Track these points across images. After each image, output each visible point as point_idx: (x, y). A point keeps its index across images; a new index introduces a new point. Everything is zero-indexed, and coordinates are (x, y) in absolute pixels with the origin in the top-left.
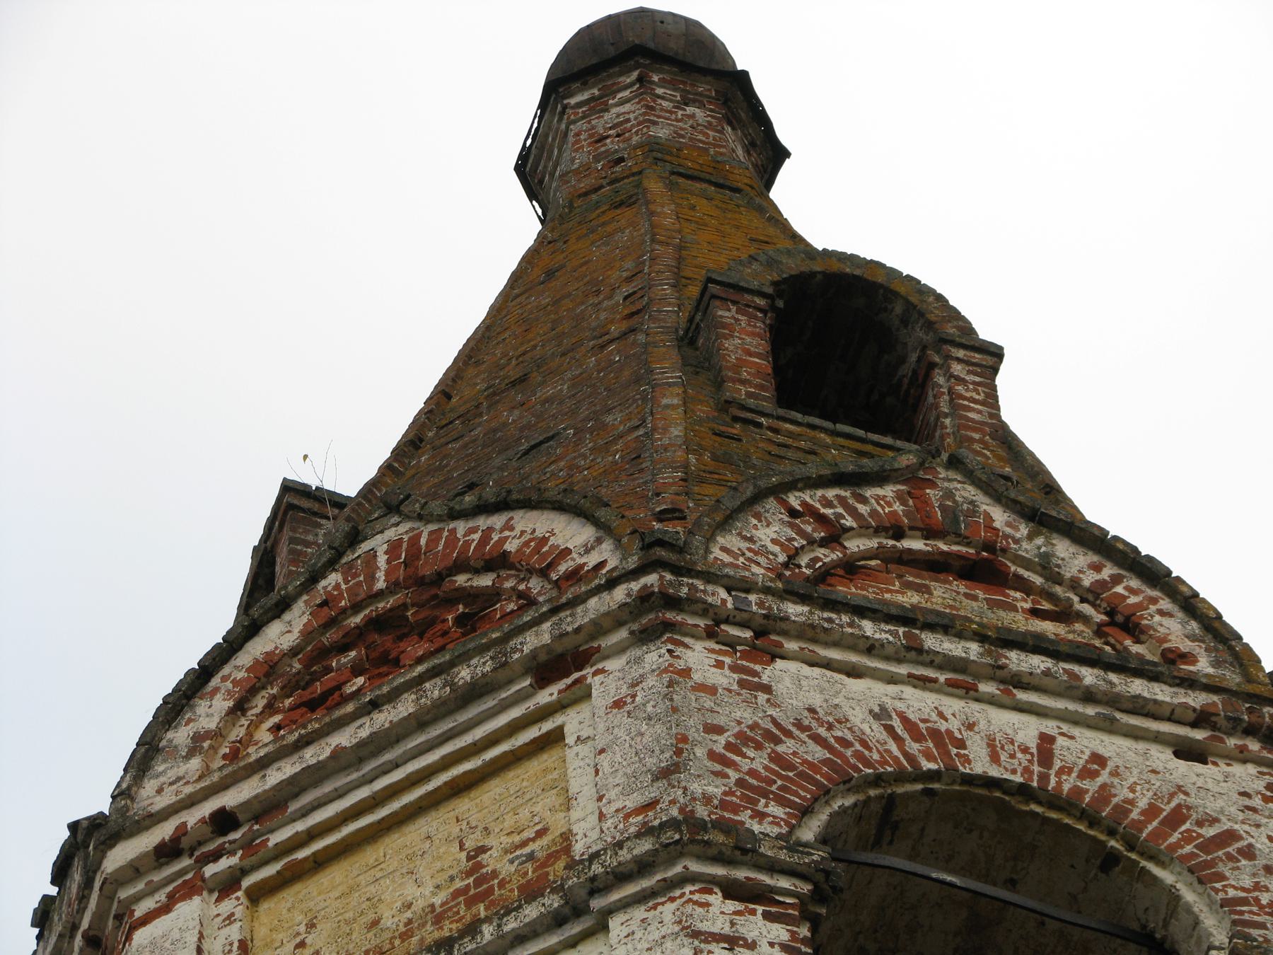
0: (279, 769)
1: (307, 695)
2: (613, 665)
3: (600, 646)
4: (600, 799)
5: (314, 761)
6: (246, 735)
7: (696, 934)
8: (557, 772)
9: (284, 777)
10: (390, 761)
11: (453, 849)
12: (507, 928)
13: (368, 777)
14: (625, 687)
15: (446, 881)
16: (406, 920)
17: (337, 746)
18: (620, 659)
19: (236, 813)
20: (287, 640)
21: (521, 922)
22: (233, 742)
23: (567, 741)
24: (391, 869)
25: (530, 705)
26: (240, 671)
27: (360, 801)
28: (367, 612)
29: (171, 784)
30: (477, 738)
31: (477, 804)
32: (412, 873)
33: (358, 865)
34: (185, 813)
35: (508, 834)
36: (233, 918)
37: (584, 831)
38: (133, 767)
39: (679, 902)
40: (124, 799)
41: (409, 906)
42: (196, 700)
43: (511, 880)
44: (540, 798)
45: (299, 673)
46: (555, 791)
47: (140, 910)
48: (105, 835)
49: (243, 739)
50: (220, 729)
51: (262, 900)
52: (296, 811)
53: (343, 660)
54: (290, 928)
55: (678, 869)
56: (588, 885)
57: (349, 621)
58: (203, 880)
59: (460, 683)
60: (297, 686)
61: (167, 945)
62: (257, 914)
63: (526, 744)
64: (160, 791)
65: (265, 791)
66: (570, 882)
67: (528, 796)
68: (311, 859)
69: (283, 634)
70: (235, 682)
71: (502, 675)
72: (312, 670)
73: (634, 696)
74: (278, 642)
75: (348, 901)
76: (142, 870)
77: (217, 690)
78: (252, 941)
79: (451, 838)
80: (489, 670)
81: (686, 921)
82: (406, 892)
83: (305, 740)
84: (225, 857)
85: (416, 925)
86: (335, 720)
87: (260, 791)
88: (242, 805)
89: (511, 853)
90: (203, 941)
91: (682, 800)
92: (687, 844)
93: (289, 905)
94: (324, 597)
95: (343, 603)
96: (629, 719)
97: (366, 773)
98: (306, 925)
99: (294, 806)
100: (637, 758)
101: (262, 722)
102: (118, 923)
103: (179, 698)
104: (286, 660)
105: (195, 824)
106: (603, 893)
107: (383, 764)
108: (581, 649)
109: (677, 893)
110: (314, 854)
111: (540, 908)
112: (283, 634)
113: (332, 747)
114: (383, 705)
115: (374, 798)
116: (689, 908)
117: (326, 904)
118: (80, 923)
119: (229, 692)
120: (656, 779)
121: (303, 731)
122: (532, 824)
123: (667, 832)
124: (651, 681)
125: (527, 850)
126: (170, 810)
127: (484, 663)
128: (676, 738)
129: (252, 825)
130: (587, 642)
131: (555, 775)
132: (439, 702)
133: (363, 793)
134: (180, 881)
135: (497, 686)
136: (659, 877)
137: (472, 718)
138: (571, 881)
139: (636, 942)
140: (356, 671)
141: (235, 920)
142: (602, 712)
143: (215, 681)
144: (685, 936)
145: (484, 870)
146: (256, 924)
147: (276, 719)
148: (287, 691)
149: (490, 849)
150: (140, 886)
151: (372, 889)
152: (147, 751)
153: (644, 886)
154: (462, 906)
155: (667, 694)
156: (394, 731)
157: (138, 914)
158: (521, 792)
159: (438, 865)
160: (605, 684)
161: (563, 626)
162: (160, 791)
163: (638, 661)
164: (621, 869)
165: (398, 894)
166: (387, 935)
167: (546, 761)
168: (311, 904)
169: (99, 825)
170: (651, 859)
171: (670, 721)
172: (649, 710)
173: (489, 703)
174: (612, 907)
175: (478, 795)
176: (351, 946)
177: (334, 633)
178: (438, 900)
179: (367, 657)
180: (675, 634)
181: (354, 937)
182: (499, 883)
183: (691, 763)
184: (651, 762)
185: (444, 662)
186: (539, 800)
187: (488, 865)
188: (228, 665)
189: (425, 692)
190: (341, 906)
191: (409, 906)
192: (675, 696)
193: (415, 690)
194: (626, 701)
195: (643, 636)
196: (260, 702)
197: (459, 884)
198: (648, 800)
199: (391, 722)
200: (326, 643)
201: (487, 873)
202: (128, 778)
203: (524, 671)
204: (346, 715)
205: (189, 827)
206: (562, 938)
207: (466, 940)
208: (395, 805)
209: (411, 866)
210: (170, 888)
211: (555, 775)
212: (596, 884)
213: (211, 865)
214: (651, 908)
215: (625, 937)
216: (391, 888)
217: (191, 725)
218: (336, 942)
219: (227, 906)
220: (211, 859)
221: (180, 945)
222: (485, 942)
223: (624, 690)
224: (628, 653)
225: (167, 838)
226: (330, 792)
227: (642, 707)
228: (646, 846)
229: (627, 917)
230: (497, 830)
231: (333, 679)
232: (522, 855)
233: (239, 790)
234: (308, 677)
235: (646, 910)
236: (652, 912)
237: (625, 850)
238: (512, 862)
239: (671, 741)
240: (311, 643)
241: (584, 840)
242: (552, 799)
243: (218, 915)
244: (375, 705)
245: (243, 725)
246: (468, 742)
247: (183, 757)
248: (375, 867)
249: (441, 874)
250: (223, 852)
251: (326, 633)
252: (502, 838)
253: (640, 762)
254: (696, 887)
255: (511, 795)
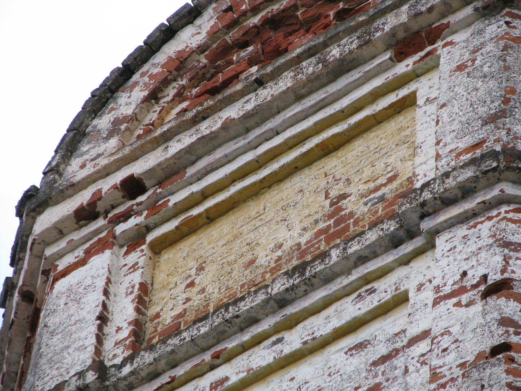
0: (179, 141)
1: (210, 85)
2: (459, 37)
3: (449, 22)
4: (438, 143)
5: (208, 132)
6: (158, 119)
7: (507, 245)
8: (410, 129)
9: (183, 147)
10: (272, 130)
11: (319, 198)
12: (350, 251)
13: (253, 144)
14: (467, 54)
15: (311, 224)
16: (276, 258)
17: (227, 118)
18: (466, 32)
19: (142, 179)
20: (197, 39)
21: (363, 244)
22: (147, 125)
23: (418, 103)
24: (269, 219)
25: (390, 75)
26: (156, 67)
27: (246, 164)
28: (263, 13)
29: (92, 160)
30: (344, 106)
31: (342, 162)
32: (285, 220)
33: (242, 218)
34: (100, 182)
35: (365, 183)
36: (136, 267)
37: (424, 172)
38: (62, 149)
39: (495, 219)
40: (53, 174)
41: (281, 246)
42: (119, 93)
43: (364, 219)
44: (394, 151)
45: (205, 67)
46: (406, 145)
47: (62, 265)
48: (35, 203)
49: (155, 122)
50: (136, 114)
51: (163, 252)
52: (192, 176)
53: (243, 54)
54: (183, 272)
55: (495, 192)
56: (419, 209)
57: (248, 22)
58: (114, 237)
59: (331, 60)
60: (203, 77)
61: (81, 290)
62: (158, 263)
63: (385, 109)
64: (83, 166)
65: (166, 160)
66: (403, 208)
67: (383, 152)
68: (204, 215)
69: (193, 35)
70: (151, 77)
71: (366, 51)
72: (217, 64)
73: (474, 60)
74: (189, 42)
75: (231, 247)
76: (64, 231)
77: (136, 83)
78: (152, 285)
79: (319, 190)
80: (355, 47)
81: (500, 235)
82: (279, 235)
83: (201, 115)
84: (133, 217)
85: (284, 261)
86: (227, 97)
87: (162, 159)
88: (147, 172)
89: (366, 197)
90: (110, 285)
91: (505, 139)
92: (503, 171)
93: (185, 254)
94: (229, 4)
95: (244, 7)
96: (468, 79)
97: (251, 141)
98: (197, 268)
99: (191, 171)
100: (471, 109)
101: (172, 109)
102: (45, 278)
103: (105, 92)
104: (196, 57)
105: (109, 190)
106: (432, 216)
107: (265, 132)
108: (434, 26)
109: (495, 213)
110: (207, 210)
111: (379, 232)
112: (193, 35)
113: (223, 120)
114: (267, 83)
115: (257, 161)
116: (503, 225)
117: (214, 251)
118: (17, 283)
119: (145, 84)
120: (485, 123)
121: (200, 108)
122: (385, 172)
123: (486, 161)
124: (490, 47)
125: (379, 193)
126: (89, 180)
127: (352, 42)
128: (506, 91)
129: (156, 189)
130: (439, 20)
131: (408, 132)
132: (312, 77)
133: (249, 157)
134: (96, 239)
135: (362, 62)
136: (479, 200)
137: (340, 90)
138: (404, 206)
139: (456, 254)
140: (251, 62)
141: (138, 268)
142: (446, 76)
143: (136, 77)
144: (498, 247)
145: (343, 213)
146: (157, 272)
147: (184, 105)
148: (195, 81)
149: (349, 196)
150: (62, 244)
151: (252, 236)
152: (75, 135)
153: (466, 208)
154: (323, 242)
155: (502, 57)
156: (275, 104)
157: (60, 268)
158: (379, 148)
159: (307, 211)
160: (451, 53)
161: (419, 7)
162: (83, 166)
163: (480, 32)
164: (447, 194)
165: (272, 238)
166: (261, 271)
167: (402, 122)
168: (202, 252)
169: (32, 196)
170: (473, 185)
171: (501, 77)
172: (485, 70)
173: (355, 75)
174: (439, 227)
175: (344, 154)
176: (231, 282)
177: (235, 32)
178: (303, 240)
179: (263, 51)
180: (514, 9)
181: (233, 275)
182: (354, 222)
183: (516, 110)
184: (482, 111)
185: (319, 43)
186: (392, 153)
187: (346, 209)
188: (147, 63)
189: (301, 69)
190: (225, 251)
191: (281, 246)
192: (508, 58)
193: (293, 68)
194: (467, 65)
195: (485, 12)
196: (171, 92)
197: (322, 225)
198: (477, 141)
199: (272, 95)
200: (229, 41)
201: (345, 215)
202: (57, 157)
203: (385, 48)
204: (236, 92)
205: (103, 192)
206: (397, 257)
207: (316, 263)
208: (275, 166)
209: (285, 215)
210: (87, 245)
211: (408, 132)
212: (426, 208)
213: (122, 224)
214: (472, 227)
215: (448, 251)
216: (267, 234)
217: (113, 112)
218: (219, 280)
219: (133, 257)
220: (122, 219)
221: (90, 289)
222: (332, 263)
223: (467, 56)
224: (473, 27)
225: (85, 203)
226: (220, 158)
227: (479, 68)
228: (469, 173)
229: (451, 235)
230: (357, 180)
231: (233, 70)
232: (374, 198)
233: (146, 160)
234: (213, 70)
235: (467, 229)
236: (473, 230)
237: (451, 179)
238: (366, 204)
239: (501, 93)
240: (216, 42)
241: (424, 179)
242: (404, 151)
243: (126, 265)
244: (260, 83)
245: (156, 111)
246: (337, 110)
247: (104, 138)
248: (256, 218)
249: (308, 218)
250: (132, 213)
251: (230, 32)
252: (360, 186)
253: (473, 111)
254: (512, 207)
255: (370, 152)
